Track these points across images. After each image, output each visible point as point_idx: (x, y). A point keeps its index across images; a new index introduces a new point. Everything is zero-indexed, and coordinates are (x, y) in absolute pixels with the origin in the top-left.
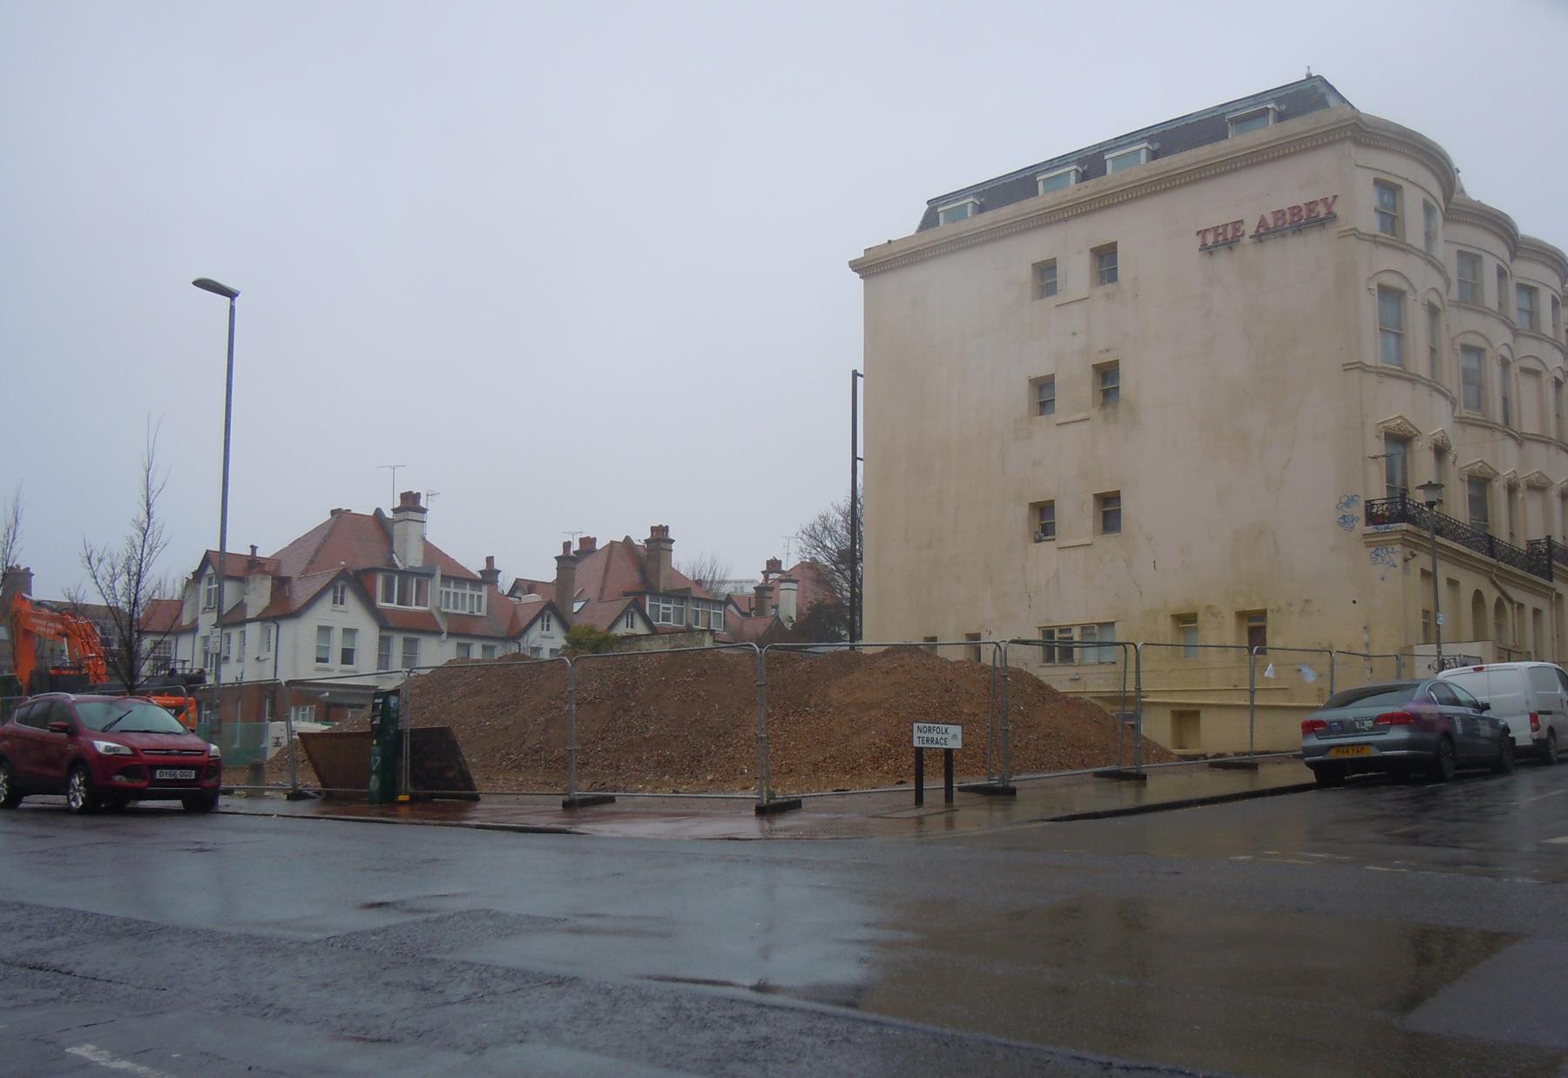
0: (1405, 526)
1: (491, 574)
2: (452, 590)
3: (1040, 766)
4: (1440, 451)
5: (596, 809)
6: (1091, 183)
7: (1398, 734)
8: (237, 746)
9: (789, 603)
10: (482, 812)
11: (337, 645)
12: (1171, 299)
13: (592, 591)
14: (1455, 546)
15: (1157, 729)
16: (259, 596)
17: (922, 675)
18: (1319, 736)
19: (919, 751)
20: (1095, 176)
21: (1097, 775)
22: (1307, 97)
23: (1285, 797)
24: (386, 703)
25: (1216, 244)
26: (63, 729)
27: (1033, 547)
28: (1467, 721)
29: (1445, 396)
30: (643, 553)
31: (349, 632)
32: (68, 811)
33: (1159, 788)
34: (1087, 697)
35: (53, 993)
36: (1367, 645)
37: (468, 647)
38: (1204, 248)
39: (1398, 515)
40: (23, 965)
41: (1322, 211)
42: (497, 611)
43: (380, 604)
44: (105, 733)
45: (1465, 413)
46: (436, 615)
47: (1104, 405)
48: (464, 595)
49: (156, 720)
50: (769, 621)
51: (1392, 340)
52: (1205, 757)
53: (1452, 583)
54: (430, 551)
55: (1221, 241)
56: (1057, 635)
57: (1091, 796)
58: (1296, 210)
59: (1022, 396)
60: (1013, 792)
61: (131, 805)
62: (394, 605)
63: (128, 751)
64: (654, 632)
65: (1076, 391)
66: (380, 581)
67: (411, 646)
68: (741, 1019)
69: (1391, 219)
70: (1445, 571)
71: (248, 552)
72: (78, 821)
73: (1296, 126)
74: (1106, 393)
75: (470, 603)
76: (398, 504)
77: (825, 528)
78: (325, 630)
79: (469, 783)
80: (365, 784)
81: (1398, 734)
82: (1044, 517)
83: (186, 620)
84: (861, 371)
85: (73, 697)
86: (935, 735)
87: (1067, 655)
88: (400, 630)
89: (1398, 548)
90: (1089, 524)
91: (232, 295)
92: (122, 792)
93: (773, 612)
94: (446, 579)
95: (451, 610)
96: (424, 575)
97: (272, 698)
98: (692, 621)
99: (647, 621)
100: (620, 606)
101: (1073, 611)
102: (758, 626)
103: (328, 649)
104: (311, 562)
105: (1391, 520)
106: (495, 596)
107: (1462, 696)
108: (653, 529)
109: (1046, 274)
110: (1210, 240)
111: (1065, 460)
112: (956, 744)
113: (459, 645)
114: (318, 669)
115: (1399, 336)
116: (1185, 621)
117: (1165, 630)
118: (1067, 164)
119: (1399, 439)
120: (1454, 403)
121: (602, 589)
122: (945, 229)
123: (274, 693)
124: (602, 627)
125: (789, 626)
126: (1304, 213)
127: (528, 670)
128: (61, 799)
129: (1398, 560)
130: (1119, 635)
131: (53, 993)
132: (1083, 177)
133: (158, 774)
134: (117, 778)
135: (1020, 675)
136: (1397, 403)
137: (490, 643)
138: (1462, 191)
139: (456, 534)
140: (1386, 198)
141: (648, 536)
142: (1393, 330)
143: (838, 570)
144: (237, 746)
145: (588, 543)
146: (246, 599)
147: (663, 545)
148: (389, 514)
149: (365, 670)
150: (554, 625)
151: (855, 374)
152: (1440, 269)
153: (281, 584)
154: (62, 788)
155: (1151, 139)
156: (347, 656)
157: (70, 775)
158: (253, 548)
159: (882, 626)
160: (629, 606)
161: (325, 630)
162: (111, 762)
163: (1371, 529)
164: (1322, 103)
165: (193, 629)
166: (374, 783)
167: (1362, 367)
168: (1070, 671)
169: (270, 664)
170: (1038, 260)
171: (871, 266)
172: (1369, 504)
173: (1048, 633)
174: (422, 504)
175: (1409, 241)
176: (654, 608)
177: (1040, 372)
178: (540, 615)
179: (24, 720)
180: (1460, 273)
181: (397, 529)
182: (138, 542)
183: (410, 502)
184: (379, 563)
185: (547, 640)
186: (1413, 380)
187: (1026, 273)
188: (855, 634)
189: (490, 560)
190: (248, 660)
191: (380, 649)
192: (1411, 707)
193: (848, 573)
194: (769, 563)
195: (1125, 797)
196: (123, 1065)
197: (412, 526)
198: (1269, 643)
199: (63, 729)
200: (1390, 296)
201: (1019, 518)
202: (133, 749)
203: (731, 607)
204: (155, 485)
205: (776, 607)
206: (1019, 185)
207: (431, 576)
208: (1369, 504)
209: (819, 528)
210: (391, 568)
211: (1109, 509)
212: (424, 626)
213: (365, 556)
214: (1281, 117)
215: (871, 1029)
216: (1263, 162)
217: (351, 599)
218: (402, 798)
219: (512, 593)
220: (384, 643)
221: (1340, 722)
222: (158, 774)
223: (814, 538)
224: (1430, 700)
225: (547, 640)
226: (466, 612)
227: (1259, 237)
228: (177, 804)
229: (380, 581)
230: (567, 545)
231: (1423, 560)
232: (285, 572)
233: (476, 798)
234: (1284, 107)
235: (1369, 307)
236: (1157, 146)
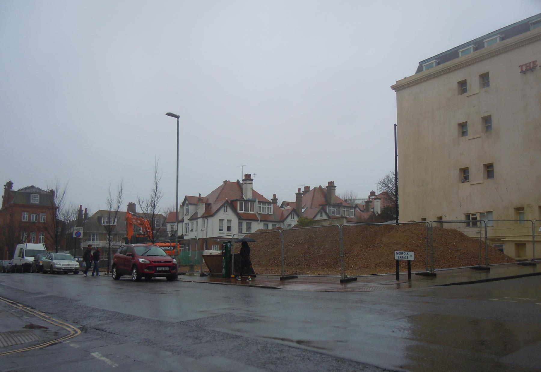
1: (275, 200)
2: (262, 206)
5: (290, 280)
6: (479, 51)
8: (196, 258)
9: (378, 207)
11: (225, 225)
13: (308, 205)
16: (201, 210)
20: (479, 49)
21: (472, 268)
23: (513, 280)
24: (226, 246)
25: (527, 70)
26: (130, 255)
27: (461, 184)
30: (326, 191)
31: (229, 221)
32: (131, 280)
35: (98, 337)
37: (267, 225)
38: (522, 72)
40: (95, 329)
43: (239, 211)
44: (142, 256)
47: (486, 131)
48: (265, 208)
49: (159, 252)
50: (370, 213)
54: (255, 193)
56: (471, 216)
59: (455, 131)
60: (435, 275)
61: (152, 278)
62: (243, 211)
64: (329, 218)
66: (239, 203)
67: (249, 225)
68: (281, 351)
71: (198, 196)
72: (135, 283)
75: (267, 210)
76: (244, 178)
78: (221, 220)
80: (221, 272)
82: (465, 174)
83: (180, 218)
85: (134, 245)
86: (403, 255)
90: (482, 175)
91: (177, 117)
92: (149, 275)
93: (372, 210)
95: (261, 213)
96: (253, 201)
97: (207, 242)
98: (343, 214)
99: (327, 214)
100: (317, 210)
102: (366, 215)
103: (224, 226)
104: (217, 198)
108: (329, 183)
109: (463, 85)
110: (524, 69)
111: (471, 152)
112: (410, 258)
113: (264, 224)
114: (220, 233)
116: (519, 210)
117: (511, 214)
118: (470, 45)
121: (312, 204)
122: (425, 72)
123: (207, 241)
131: (98, 337)
132: (476, 49)
133: (158, 269)
134: (146, 270)
135: (455, 232)
137: (274, 223)
139: (263, 187)
141: (327, 185)
144: (196, 258)
145: (307, 188)
146: (198, 211)
148: (241, 182)
149: (235, 233)
151: (395, 125)
153: (208, 206)
154: (130, 274)
155: (501, 34)
156: (229, 229)
157: (132, 270)
158: (200, 194)
160: (320, 210)
161: (221, 220)
162: (144, 265)
165: (182, 221)
166: (224, 271)
168: (476, 229)
171: (398, 88)
173: (468, 216)
174: (252, 178)
177: (462, 121)
178: (290, 213)
179: (121, 253)
181: (244, 186)
182: (154, 196)
183: (248, 177)
184: (238, 198)
185: (292, 222)
187: (455, 86)
188: (397, 219)
189: (275, 195)
190: (198, 231)
191: (239, 226)
194: (371, 193)
195: (483, 276)
196: (103, 358)
199: (130, 255)
201: (455, 174)
203: (357, 209)
204: (158, 178)
205: (373, 208)
206: (453, 54)
207: (255, 201)
209: (386, 181)
213: (234, 196)
215: (319, 355)
217: (229, 210)
218: (232, 276)
219: (282, 206)
220: (240, 224)
222: (158, 269)
223: (385, 183)
228: (165, 278)
229: (239, 203)
230: (299, 190)
232: (210, 202)
236: (503, 35)
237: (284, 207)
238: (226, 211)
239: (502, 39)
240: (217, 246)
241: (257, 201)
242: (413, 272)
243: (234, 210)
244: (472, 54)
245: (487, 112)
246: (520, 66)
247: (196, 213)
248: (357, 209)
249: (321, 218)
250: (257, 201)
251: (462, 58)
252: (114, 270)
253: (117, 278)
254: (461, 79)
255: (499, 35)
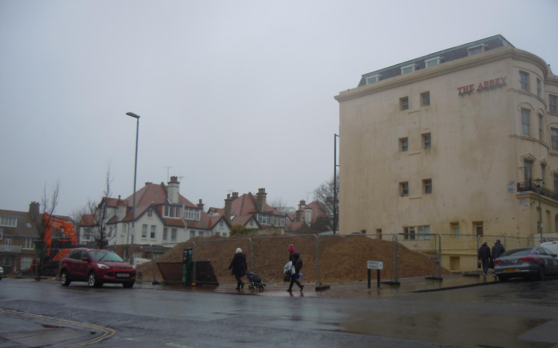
0: (531, 192)
1: (200, 206)
2: (189, 211)
3: (405, 276)
4: (543, 165)
7: (526, 265)
9: (309, 217)
10: (220, 289)
12: (446, 111)
14: (549, 199)
15: (445, 263)
16: (122, 213)
17: (366, 245)
18: (500, 265)
19: (369, 271)
22: (495, 42)
24: (188, 253)
25: (465, 93)
26: (86, 260)
27: (400, 198)
28: (549, 260)
29: (545, 146)
30: (256, 198)
31: (154, 227)
32: (88, 287)
33: (446, 283)
34: (420, 252)
36: (518, 234)
39: (528, 188)
41: (501, 82)
42: (197, 217)
44: (100, 261)
45: (552, 151)
46: (184, 221)
51: (526, 127)
52: (461, 272)
53: (548, 212)
54: (181, 198)
55: (466, 92)
56: (409, 230)
57: (423, 285)
58: (492, 81)
59: (396, 145)
62: (168, 217)
63: (108, 267)
64: (261, 228)
65: (415, 142)
69: (526, 85)
70: (544, 207)
71: (117, 198)
73: (492, 52)
74: (426, 144)
75: (194, 216)
76: (169, 181)
77: (323, 189)
78: (145, 226)
79: (216, 280)
80: (181, 280)
81: (526, 265)
82: (404, 188)
84: (338, 134)
85: (88, 250)
86: (374, 265)
87: (413, 237)
88: (170, 226)
89: (528, 200)
91: (138, 117)
93: (303, 220)
94: (187, 208)
95: (188, 219)
96: (179, 206)
98: (273, 223)
99: (258, 223)
101: (414, 221)
102: (296, 225)
103: (146, 231)
105: (526, 190)
106: (203, 214)
107: (547, 252)
108: (259, 190)
109: (404, 102)
110: (462, 91)
111: (411, 167)
113: (173, 229)
114: (143, 240)
115: (529, 125)
116: (455, 225)
117: (447, 228)
118: (412, 63)
119: (529, 161)
120: (548, 148)
122: (368, 86)
124: (242, 224)
125: (309, 225)
126: (495, 82)
127: (217, 240)
128: (85, 284)
129: (528, 204)
130: (431, 231)
132: (417, 68)
136: (528, 149)
137: (201, 231)
138: (551, 72)
139: (190, 192)
140: (523, 78)
142: (526, 123)
143: (328, 205)
145: (235, 194)
147: (263, 195)
148: (166, 184)
149: (159, 241)
150: (225, 226)
151: (335, 135)
152: (543, 102)
154: (86, 279)
155: (441, 55)
156: (153, 235)
158: (120, 196)
159: (346, 227)
161: (145, 226)
162: (103, 271)
163: (519, 193)
164: (501, 45)
166: (184, 279)
167: (515, 136)
169: (126, 238)
170: (402, 97)
171: (342, 98)
172: (518, 185)
174: (178, 180)
175: (532, 92)
176: (260, 218)
177: (403, 136)
178: (219, 221)
180: (550, 102)
181: (169, 190)
183: (174, 180)
186: (534, 141)
187: (397, 101)
188: (335, 228)
189: (200, 201)
192: (530, 256)
193: (332, 207)
195: (436, 286)
197: (175, 189)
198: (484, 234)
199: (86, 260)
200: (526, 111)
201: (395, 187)
202: (110, 267)
203: (287, 218)
204: (110, 179)
205: (304, 218)
206: (394, 71)
207: (181, 206)
208: (518, 185)
209: (321, 190)
210: (167, 204)
211: (427, 185)
212: (178, 225)
213: (159, 199)
214: (486, 49)
216: (481, 65)
218: (194, 284)
220: (165, 231)
221: (507, 261)
223: (319, 193)
224: (536, 253)
225: (223, 230)
226: (193, 219)
227: (479, 91)
228: (121, 285)
230: (229, 195)
231: (537, 204)
233: (218, 285)
234: (487, 45)
235: (518, 116)
236: (443, 58)
237: (211, 213)
238: (150, 215)
239: (442, 61)
240: (140, 254)
241: (184, 205)
242: (382, 280)
243: (159, 215)
244: (414, 73)
245: (426, 129)
246: (458, 89)
247: (115, 217)
248: (287, 218)
249: (251, 226)
250: (184, 205)
251: (403, 76)
252: (64, 276)
253: (66, 285)
254: (402, 96)
255: (439, 57)
